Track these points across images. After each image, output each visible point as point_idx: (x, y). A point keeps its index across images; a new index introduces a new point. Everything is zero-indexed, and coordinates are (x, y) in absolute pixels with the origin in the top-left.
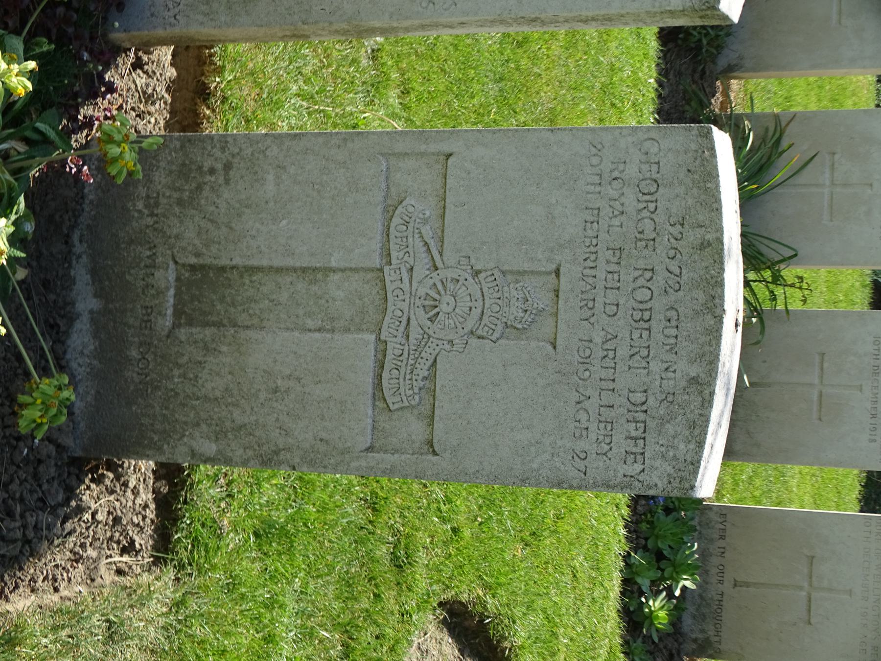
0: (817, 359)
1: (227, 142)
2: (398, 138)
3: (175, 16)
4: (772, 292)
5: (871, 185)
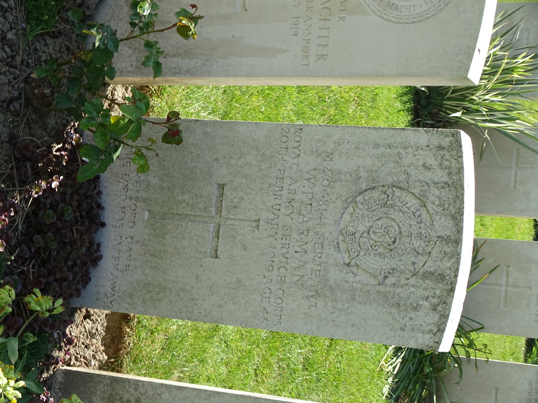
0: (494, 391)
1: (138, 385)
2: (241, 400)
3: (111, 302)
4: (468, 352)
5: (531, 288)
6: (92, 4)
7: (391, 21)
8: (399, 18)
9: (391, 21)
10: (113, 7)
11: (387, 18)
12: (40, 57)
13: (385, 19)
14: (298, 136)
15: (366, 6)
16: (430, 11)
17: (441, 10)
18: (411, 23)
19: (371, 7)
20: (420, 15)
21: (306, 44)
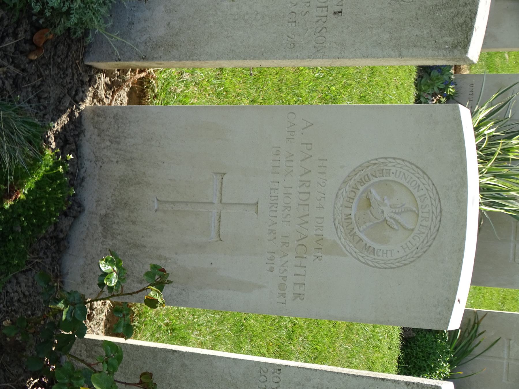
6: (65, 227)
7: (367, 264)
8: (377, 262)
9: (367, 264)
10: (88, 225)
11: (364, 261)
12: (12, 298)
13: (362, 262)
14: (277, 377)
15: (342, 246)
16: (408, 257)
17: (419, 257)
18: (388, 268)
19: (348, 248)
20: (397, 261)
21: (283, 282)
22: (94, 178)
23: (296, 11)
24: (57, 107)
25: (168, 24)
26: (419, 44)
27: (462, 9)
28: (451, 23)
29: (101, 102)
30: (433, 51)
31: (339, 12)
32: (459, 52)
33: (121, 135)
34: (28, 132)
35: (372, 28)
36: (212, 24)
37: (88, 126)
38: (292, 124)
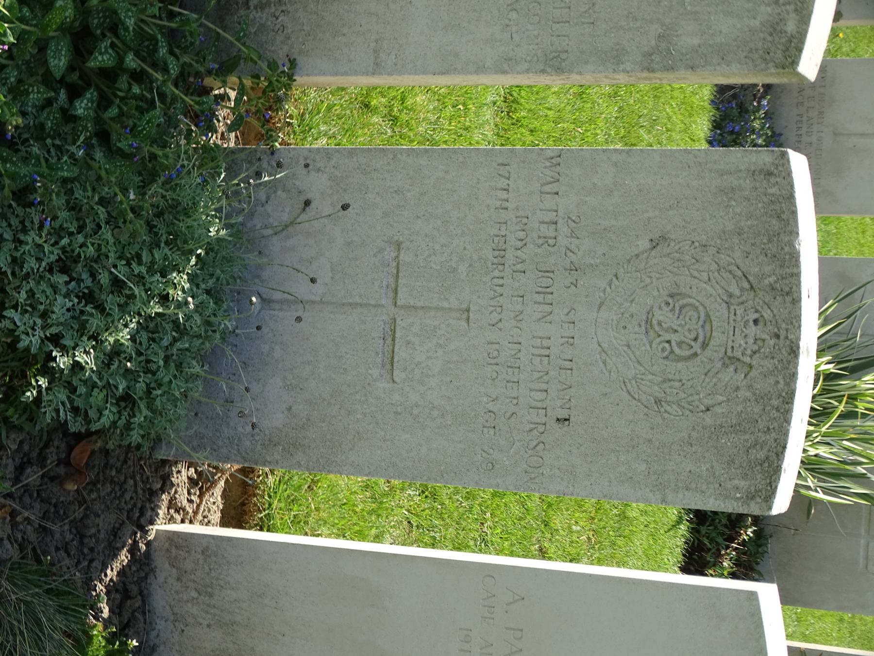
22: (171, 649)
23: (495, 410)
24: (110, 544)
25: (290, 409)
26: (693, 486)
27: (762, 437)
28: (745, 457)
29: (181, 512)
30: (716, 499)
31: (566, 420)
32: (757, 506)
33: (214, 582)
34: (67, 608)
35: (618, 451)
36: (359, 416)
37: (160, 562)
38: (489, 595)
